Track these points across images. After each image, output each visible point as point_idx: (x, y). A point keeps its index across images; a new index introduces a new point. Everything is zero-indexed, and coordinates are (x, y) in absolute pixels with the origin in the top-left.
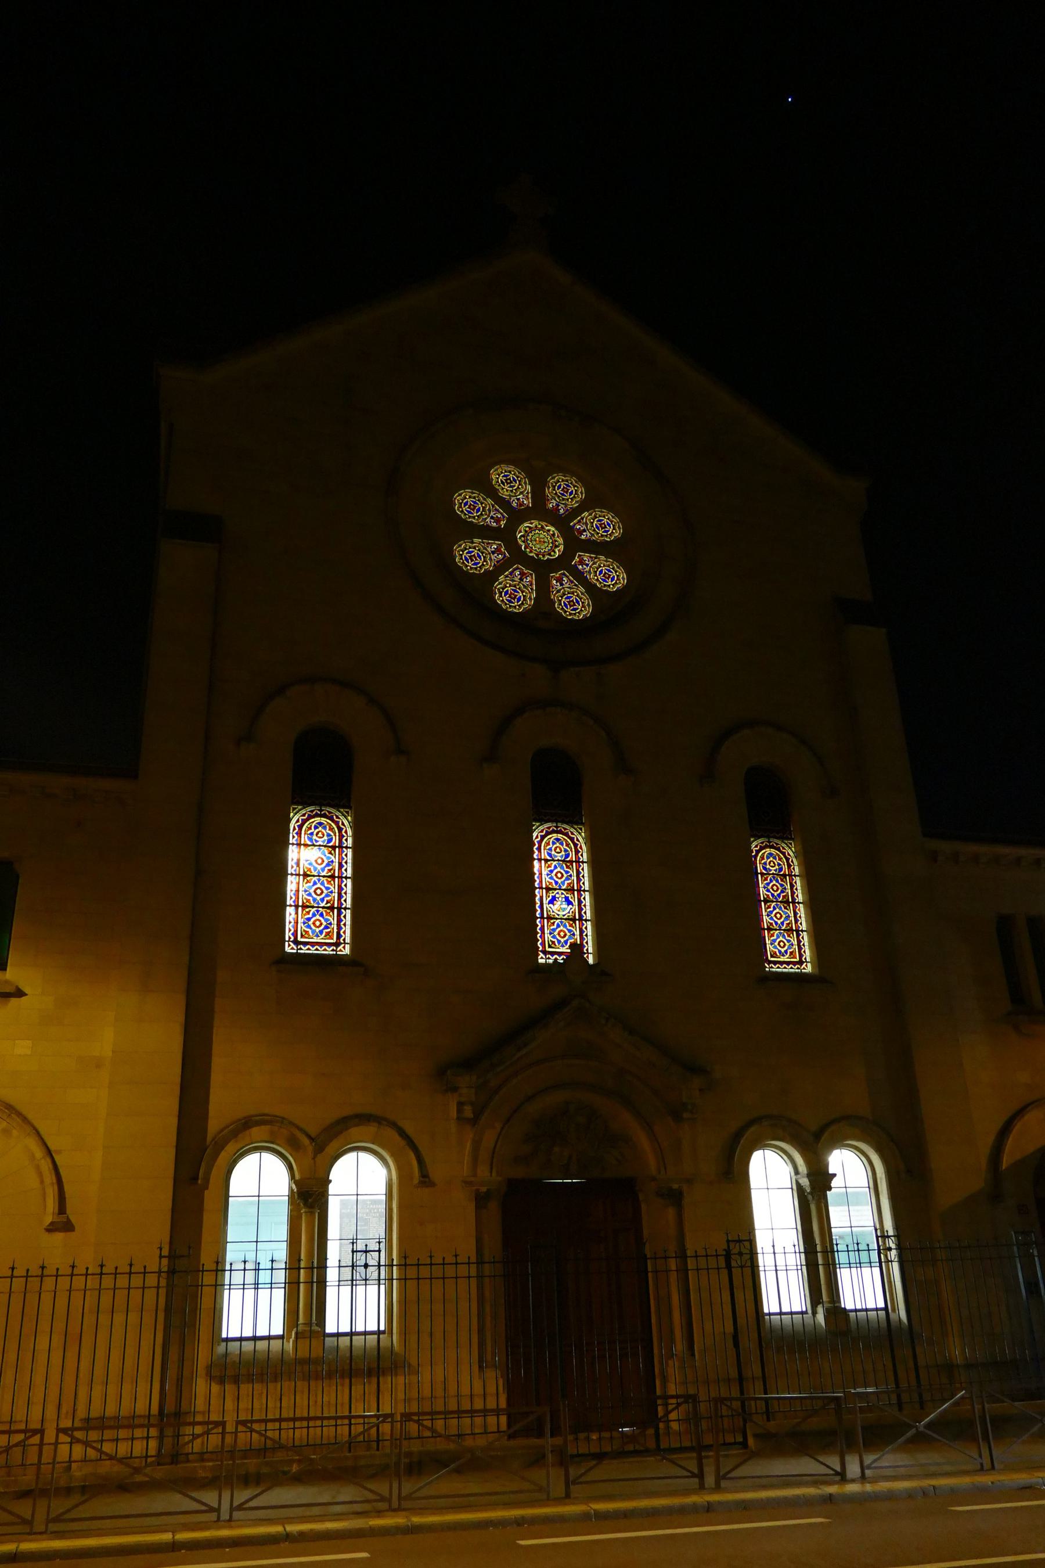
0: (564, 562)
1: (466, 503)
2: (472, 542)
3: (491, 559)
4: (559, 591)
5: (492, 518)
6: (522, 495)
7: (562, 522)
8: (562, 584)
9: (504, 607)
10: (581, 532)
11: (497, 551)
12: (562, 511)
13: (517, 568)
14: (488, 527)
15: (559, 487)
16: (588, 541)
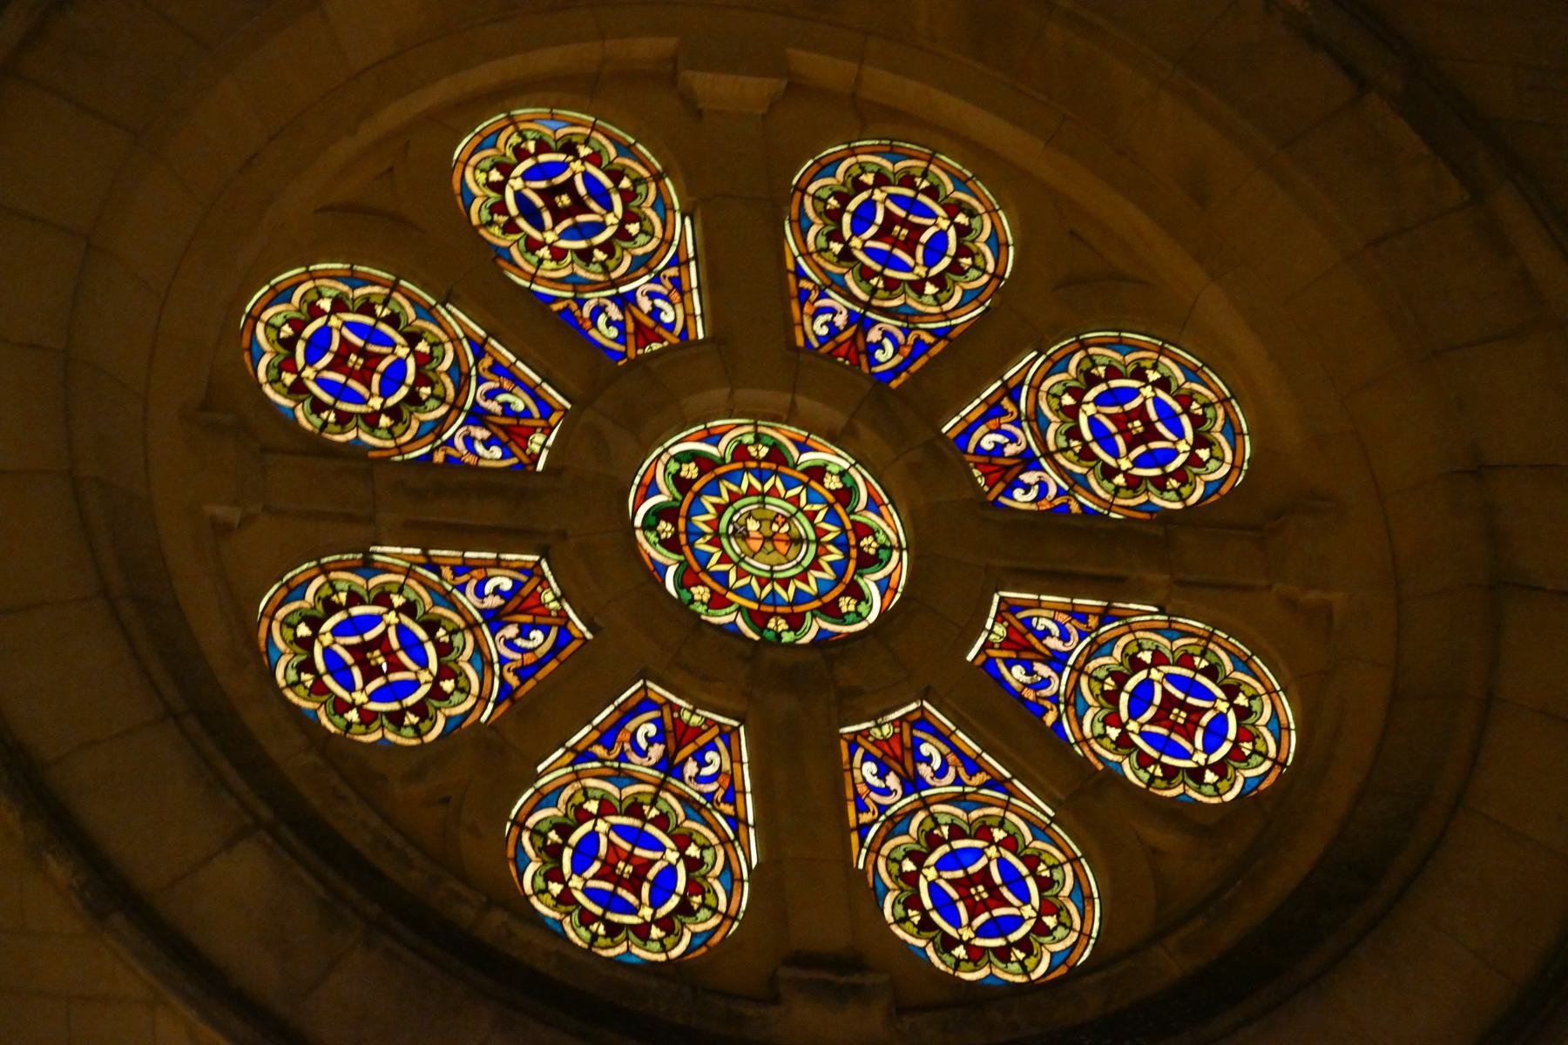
0: (915, 649)
1: (308, 328)
2: (368, 567)
3: (481, 659)
4: (897, 824)
5: (477, 416)
6: (646, 270)
7: (897, 416)
8: (913, 784)
9: (578, 936)
10: (1007, 472)
11: (518, 605)
12: (886, 356)
13: (645, 704)
14: (459, 475)
15: (863, 218)
16: (1054, 521)
